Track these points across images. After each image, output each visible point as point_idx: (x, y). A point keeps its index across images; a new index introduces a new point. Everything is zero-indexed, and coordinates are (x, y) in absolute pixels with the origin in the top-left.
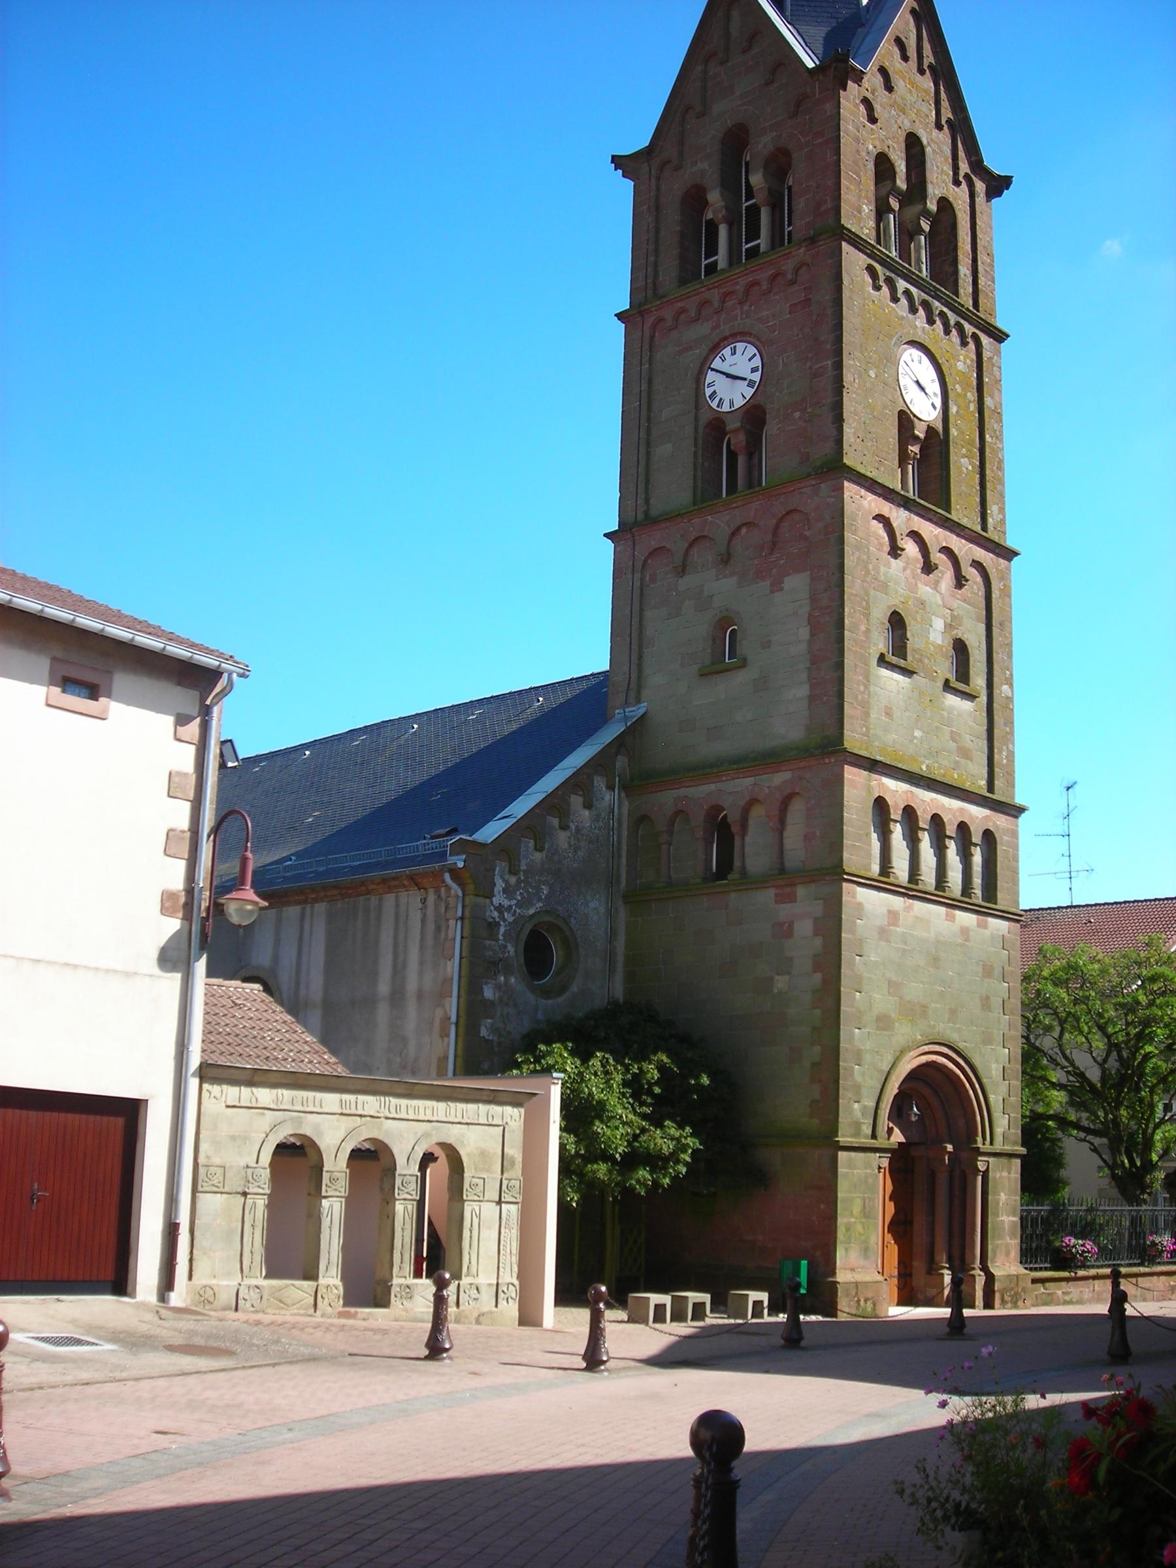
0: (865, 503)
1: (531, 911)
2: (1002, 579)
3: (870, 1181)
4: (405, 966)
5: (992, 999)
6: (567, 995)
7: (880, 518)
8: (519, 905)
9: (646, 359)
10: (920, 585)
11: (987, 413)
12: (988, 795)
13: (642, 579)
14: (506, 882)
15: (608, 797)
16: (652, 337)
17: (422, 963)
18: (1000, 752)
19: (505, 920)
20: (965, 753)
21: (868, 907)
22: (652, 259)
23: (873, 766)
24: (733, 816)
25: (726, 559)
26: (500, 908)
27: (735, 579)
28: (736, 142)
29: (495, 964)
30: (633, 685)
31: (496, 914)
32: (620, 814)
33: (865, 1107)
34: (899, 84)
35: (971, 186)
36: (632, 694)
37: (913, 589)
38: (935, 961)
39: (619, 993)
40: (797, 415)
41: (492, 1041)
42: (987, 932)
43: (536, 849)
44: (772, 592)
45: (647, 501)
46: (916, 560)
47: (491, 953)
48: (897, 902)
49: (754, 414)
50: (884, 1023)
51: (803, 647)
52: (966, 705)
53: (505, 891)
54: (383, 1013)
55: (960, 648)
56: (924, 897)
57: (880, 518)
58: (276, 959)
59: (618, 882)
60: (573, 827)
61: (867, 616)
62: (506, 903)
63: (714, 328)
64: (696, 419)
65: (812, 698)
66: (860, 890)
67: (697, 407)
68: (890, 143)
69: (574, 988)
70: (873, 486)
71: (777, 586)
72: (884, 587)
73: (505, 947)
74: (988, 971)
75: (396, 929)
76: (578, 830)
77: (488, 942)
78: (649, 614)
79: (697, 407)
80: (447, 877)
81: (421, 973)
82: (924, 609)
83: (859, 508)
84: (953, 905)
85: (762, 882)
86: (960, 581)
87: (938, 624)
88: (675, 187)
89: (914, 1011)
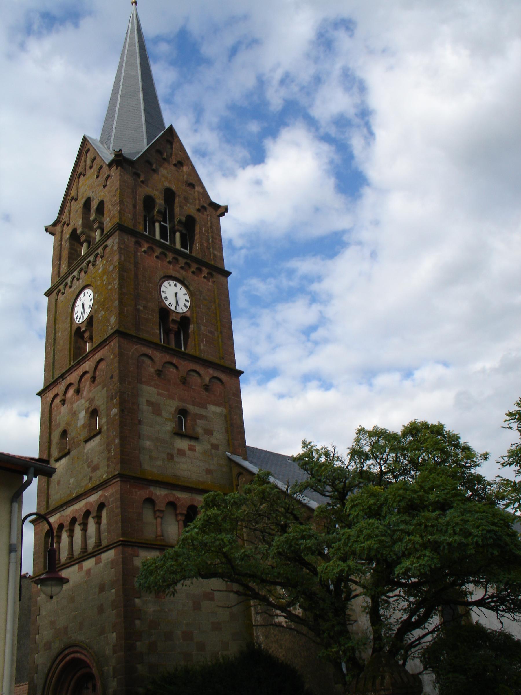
49: (90, 320)
88: (67, 231)
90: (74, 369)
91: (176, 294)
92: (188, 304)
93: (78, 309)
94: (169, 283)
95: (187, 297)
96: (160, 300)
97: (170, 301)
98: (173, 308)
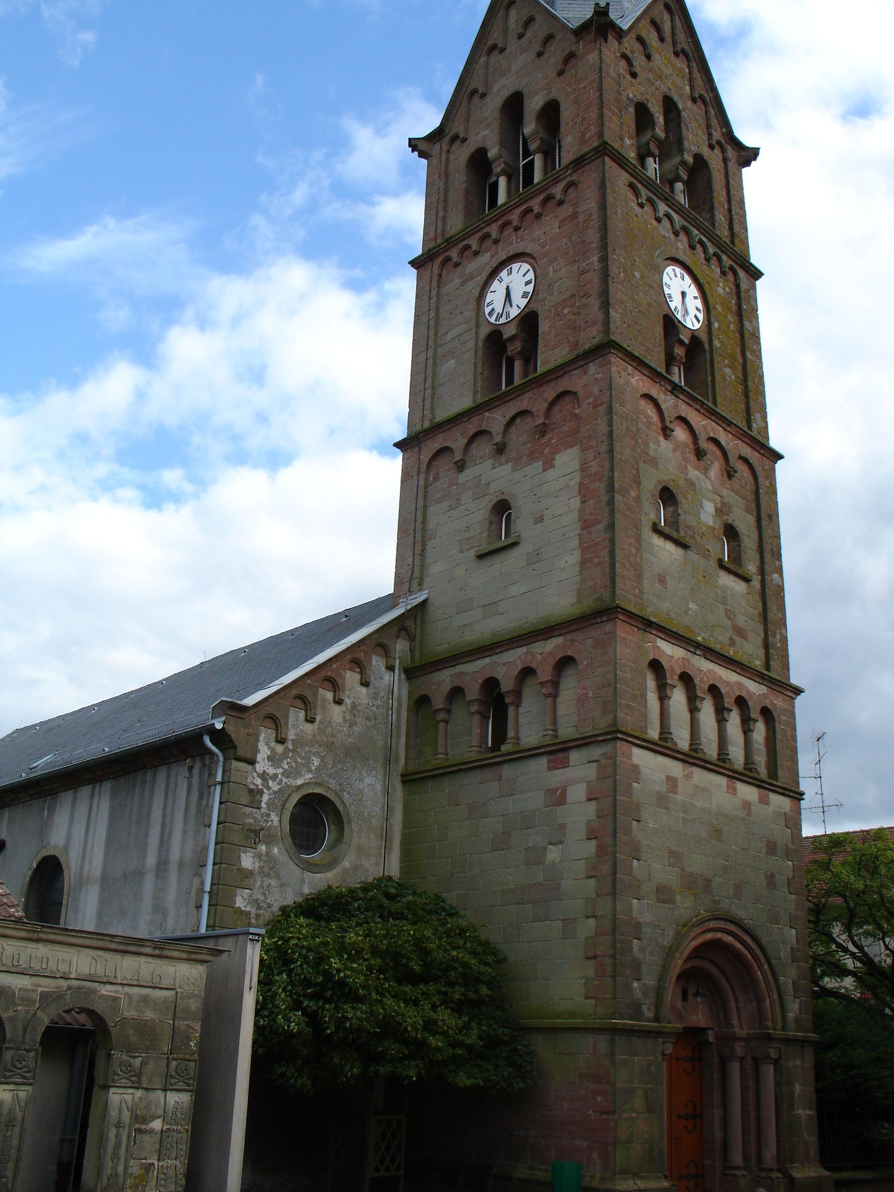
0: (633, 381)
1: (300, 782)
2: (767, 478)
3: (653, 1069)
4: (170, 835)
5: (777, 876)
6: (338, 870)
7: (647, 396)
8: (286, 774)
9: (434, 293)
10: (690, 468)
11: (747, 335)
12: (764, 671)
13: (426, 479)
14: (273, 750)
15: (387, 677)
16: (440, 275)
17: (184, 832)
18: (774, 636)
19: (269, 788)
20: (740, 632)
21: (644, 771)
22: (441, 214)
23: (648, 625)
24: (507, 685)
25: (501, 449)
26: (264, 776)
27: (510, 464)
28: (514, 107)
29: (256, 833)
30: (417, 573)
31: (259, 781)
32: (400, 696)
33: (645, 985)
34: (657, 58)
35: (723, 151)
36: (415, 583)
37: (684, 470)
38: (717, 833)
39: (394, 869)
40: (566, 311)
41: (249, 913)
42: (770, 809)
43: (307, 720)
44: (544, 470)
45: (433, 409)
46: (686, 445)
47: (252, 821)
48: (676, 768)
49: (529, 320)
50: (664, 895)
51: (575, 516)
52: (739, 586)
53: (270, 758)
54: (149, 882)
55: (731, 532)
56: (705, 765)
57: (647, 396)
58: (69, 838)
59: (397, 760)
60: (348, 701)
61: (638, 483)
62: (271, 771)
63: (492, 257)
64: (477, 333)
65: (584, 562)
66: (636, 751)
67: (478, 325)
68: (648, 97)
69: (346, 864)
70: (639, 363)
71: (549, 464)
72: (653, 462)
73: (268, 815)
74: (772, 849)
75: (166, 799)
76: (354, 706)
77: (248, 810)
78: (431, 510)
79: (478, 325)
80: (207, 740)
81: (183, 843)
82: (694, 490)
83: (627, 383)
84: (734, 775)
85: (531, 754)
86: (730, 473)
87: (709, 508)
88: (462, 155)
89: (698, 885)
90: (698, 407)
91: (683, 294)
92: (701, 316)
93: (495, 297)
94: (674, 270)
95: (699, 303)
96: (662, 299)
97: (675, 303)
98: (679, 317)
